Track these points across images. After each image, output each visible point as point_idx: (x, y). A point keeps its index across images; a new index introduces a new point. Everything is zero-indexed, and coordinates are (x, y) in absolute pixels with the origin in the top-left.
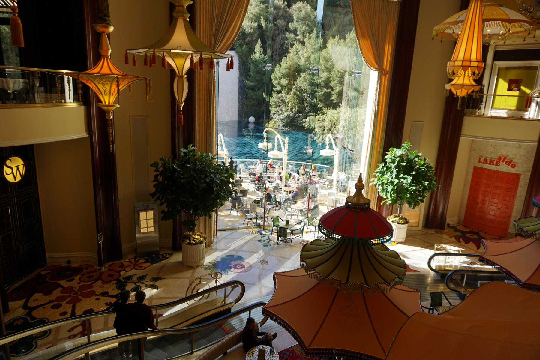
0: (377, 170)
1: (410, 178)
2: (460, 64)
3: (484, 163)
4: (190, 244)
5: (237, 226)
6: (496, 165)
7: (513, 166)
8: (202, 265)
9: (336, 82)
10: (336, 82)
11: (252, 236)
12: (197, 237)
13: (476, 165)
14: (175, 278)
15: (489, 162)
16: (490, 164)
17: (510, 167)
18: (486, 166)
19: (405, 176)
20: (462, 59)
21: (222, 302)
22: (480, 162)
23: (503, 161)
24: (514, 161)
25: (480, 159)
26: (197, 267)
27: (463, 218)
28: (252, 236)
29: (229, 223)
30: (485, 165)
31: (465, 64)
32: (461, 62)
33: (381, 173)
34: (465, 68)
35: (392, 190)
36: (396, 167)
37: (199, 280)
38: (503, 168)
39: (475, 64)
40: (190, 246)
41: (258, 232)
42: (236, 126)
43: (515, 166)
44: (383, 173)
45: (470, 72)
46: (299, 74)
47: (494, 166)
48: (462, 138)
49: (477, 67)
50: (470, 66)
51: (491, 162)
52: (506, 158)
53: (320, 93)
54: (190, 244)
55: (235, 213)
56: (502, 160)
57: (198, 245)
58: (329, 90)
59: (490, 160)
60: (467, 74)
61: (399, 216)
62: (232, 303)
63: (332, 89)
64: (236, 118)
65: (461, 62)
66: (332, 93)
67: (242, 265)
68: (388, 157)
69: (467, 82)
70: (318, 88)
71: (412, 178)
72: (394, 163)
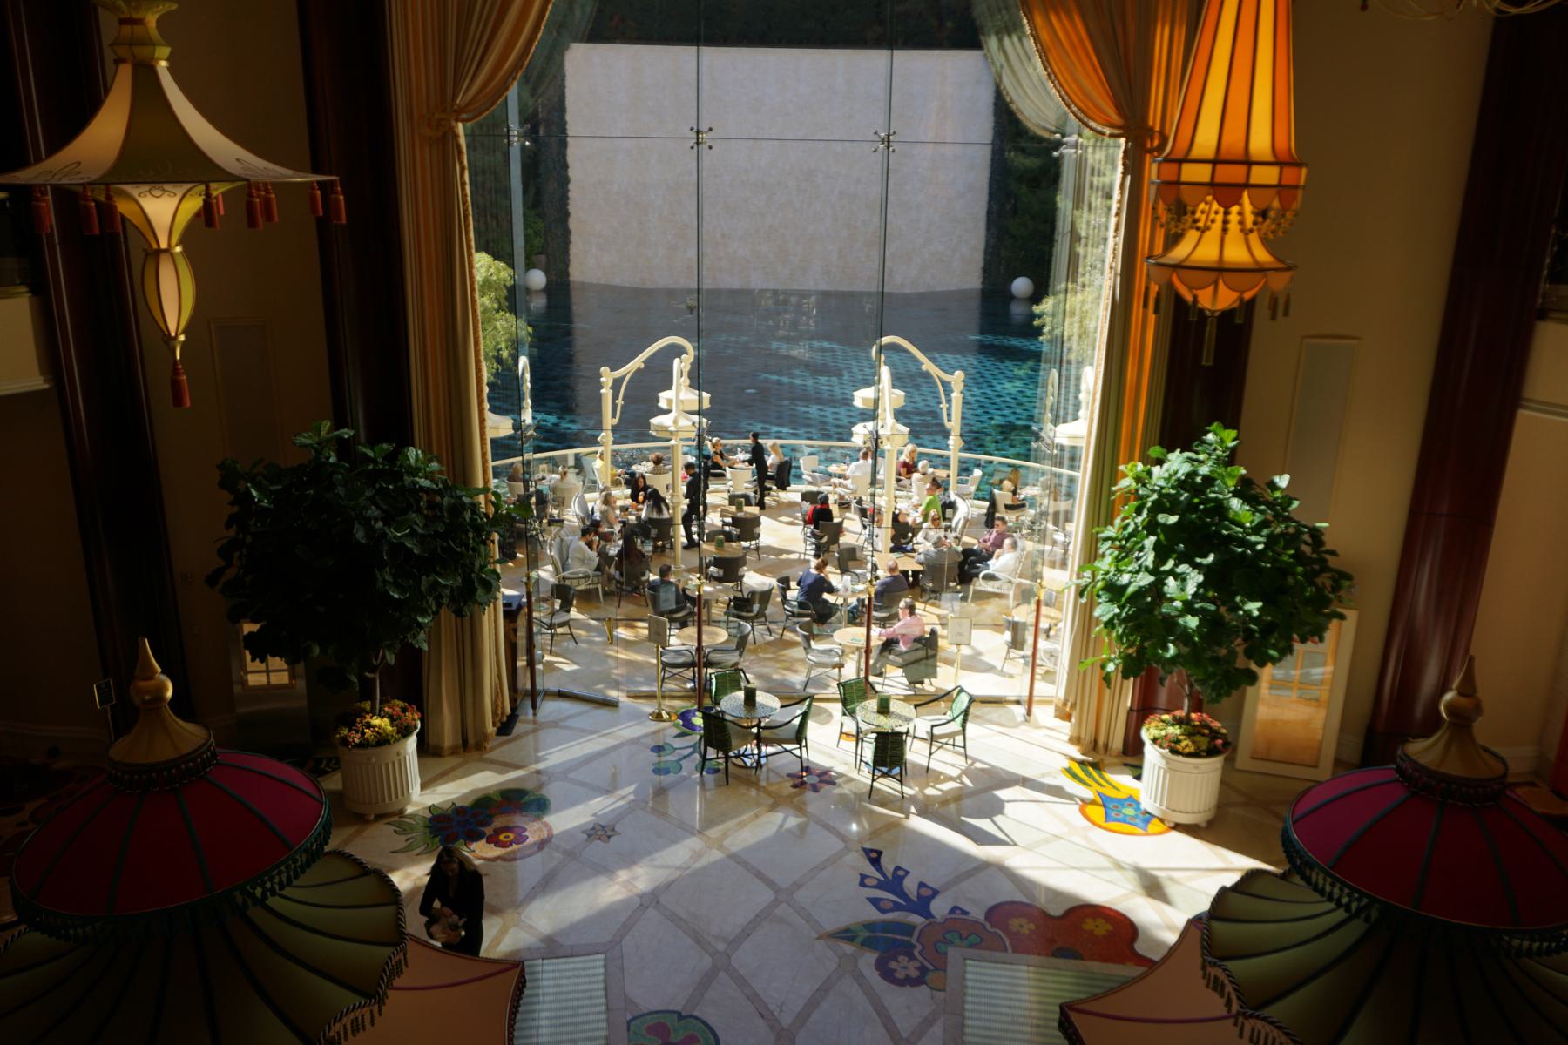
2: (1202, 173)
8: (401, 813)
20: (1210, 154)
27: (1552, 756)
31: (1229, 174)
32: (1208, 167)
34: (1227, 193)
39: (1266, 175)
42: (975, 304)
45: (1248, 208)
49: (1279, 186)
50: (1247, 185)
57: (370, 751)
60: (1234, 217)
64: (972, 280)
65: (1208, 167)
69: (1236, 253)
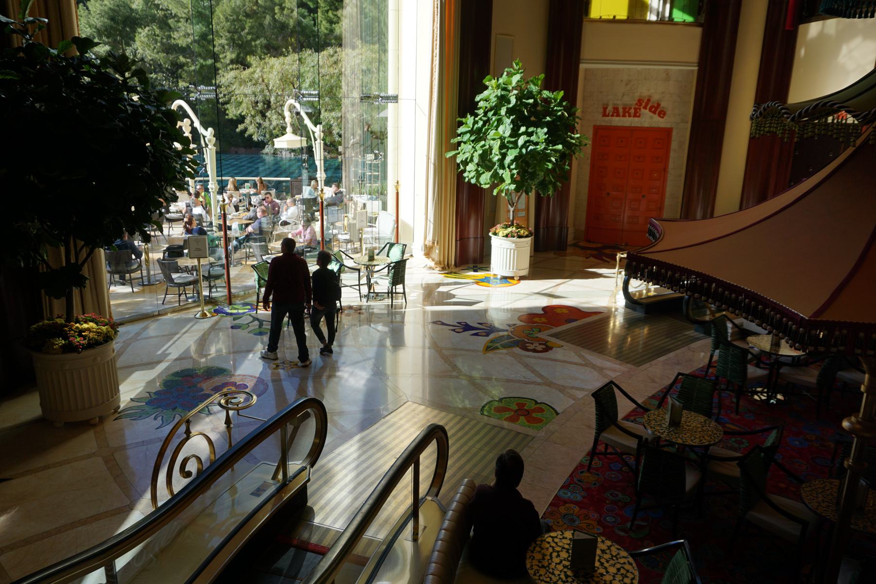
0: (461, 130)
1: (541, 133)
3: (612, 116)
4: (70, 348)
5: (148, 309)
6: (635, 116)
7: (662, 114)
9: (223, 41)
10: (223, 41)
11: (206, 324)
12: (85, 326)
13: (598, 123)
14: (46, 467)
15: (621, 114)
16: (624, 116)
17: (656, 118)
18: (617, 121)
19: (531, 130)
21: (274, 477)
22: (605, 115)
23: (645, 108)
24: (663, 104)
25: (605, 109)
26: (102, 419)
27: (583, 228)
28: (206, 324)
29: (121, 309)
30: (614, 118)
33: (471, 132)
35: (516, 159)
36: (510, 112)
37: (183, 428)
38: (648, 120)
40: (75, 355)
41: (217, 312)
43: (665, 114)
44: (479, 135)
46: (134, 31)
47: (632, 118)
48: (583, 66)
51: (626, 112)
52: (649, 100)
53: (193, 68)
54: (70, 348)
55: (127, 289)
56: (644, 104)
57: (99, 349)
58: (210, 62)
59: (624, 109)
61: (512, 225)
62: (303, 469)
63: (215, 57)
66: (218, 65)
67: (234, 384)
68: (488, 96)
70: (184, 57)
71: (545, 130)
72: (509, 102)
